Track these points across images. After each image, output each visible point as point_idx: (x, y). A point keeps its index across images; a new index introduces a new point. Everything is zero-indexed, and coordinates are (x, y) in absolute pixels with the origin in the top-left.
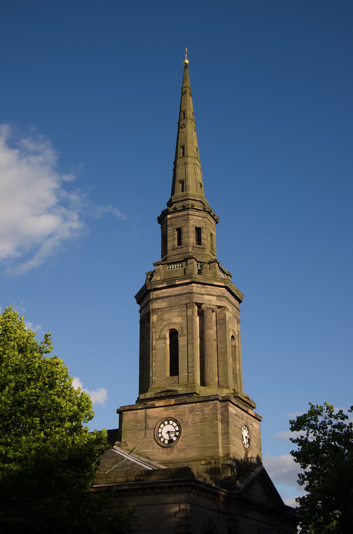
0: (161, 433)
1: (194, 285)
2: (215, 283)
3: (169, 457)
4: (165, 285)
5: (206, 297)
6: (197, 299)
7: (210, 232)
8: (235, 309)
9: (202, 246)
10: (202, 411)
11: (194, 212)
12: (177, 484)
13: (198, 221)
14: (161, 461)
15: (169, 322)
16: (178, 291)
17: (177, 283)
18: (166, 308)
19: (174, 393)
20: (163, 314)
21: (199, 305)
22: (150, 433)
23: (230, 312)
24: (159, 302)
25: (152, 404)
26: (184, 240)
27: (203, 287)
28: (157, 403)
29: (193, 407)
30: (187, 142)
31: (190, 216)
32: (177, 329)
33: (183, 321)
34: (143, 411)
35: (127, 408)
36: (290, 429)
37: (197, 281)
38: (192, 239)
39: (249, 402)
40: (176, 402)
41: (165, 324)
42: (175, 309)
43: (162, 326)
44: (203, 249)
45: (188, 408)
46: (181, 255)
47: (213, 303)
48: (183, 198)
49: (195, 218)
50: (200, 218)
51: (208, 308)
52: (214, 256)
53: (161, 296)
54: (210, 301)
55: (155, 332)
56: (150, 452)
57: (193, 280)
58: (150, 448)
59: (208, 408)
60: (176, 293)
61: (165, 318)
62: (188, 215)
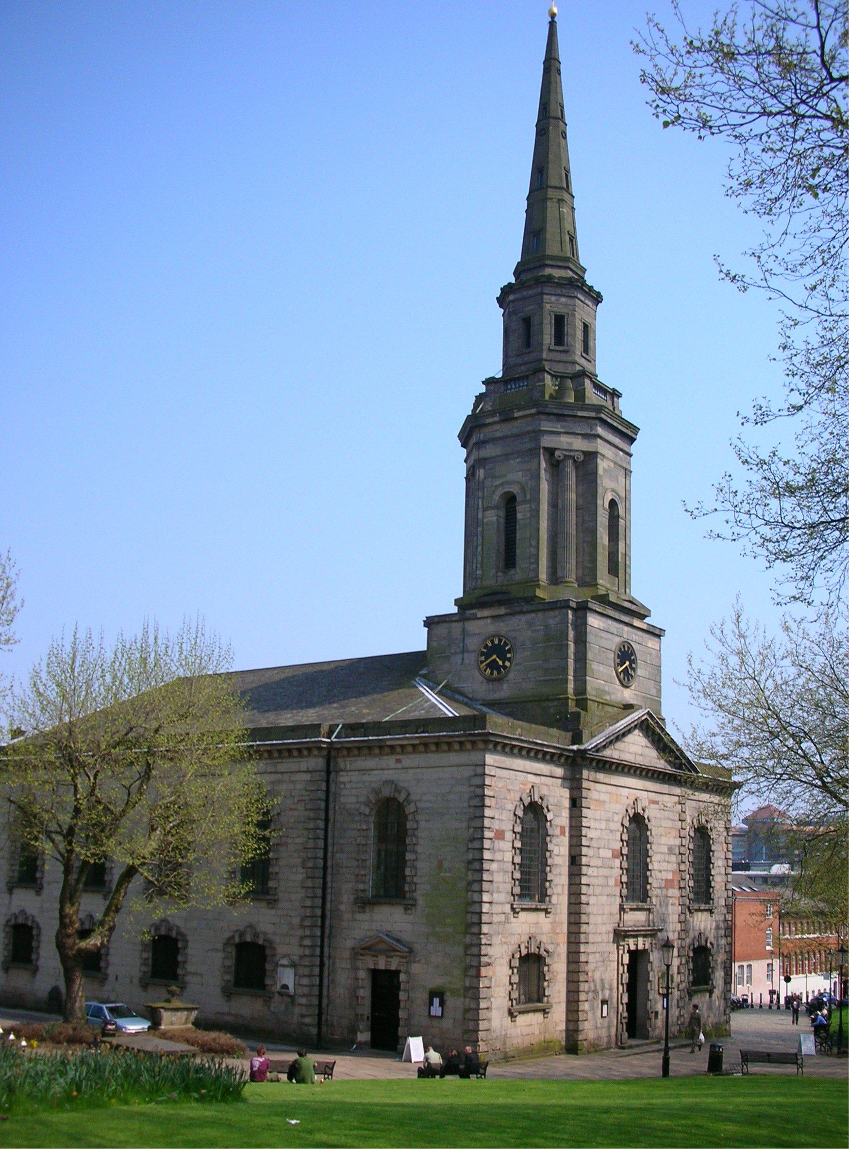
2: (580, 414)
4: (496, 419)
6: (547, 441)
8: (621, 453)
9: (565, 348)
12: (470, 738)
15: (503, 480)
17: (516, 415)
19: (505, 597)
21: (550, 452)
25: (473, 614)
32: (515, 492)
34: (459, 625)
35: (436, 620)
37: (548, 410)
38: (548, 338)
39: (633, 607)
40: (508, 611)
42: (513, 459)
46: (530, 365)
47: (575, 447)
48: (537, 264)
51: (565, 456)
54: (571, 444)
55: (483, 498)
57: (541, 409)
59: (553, 619)
60: (515, 431)
62: (542, 294)
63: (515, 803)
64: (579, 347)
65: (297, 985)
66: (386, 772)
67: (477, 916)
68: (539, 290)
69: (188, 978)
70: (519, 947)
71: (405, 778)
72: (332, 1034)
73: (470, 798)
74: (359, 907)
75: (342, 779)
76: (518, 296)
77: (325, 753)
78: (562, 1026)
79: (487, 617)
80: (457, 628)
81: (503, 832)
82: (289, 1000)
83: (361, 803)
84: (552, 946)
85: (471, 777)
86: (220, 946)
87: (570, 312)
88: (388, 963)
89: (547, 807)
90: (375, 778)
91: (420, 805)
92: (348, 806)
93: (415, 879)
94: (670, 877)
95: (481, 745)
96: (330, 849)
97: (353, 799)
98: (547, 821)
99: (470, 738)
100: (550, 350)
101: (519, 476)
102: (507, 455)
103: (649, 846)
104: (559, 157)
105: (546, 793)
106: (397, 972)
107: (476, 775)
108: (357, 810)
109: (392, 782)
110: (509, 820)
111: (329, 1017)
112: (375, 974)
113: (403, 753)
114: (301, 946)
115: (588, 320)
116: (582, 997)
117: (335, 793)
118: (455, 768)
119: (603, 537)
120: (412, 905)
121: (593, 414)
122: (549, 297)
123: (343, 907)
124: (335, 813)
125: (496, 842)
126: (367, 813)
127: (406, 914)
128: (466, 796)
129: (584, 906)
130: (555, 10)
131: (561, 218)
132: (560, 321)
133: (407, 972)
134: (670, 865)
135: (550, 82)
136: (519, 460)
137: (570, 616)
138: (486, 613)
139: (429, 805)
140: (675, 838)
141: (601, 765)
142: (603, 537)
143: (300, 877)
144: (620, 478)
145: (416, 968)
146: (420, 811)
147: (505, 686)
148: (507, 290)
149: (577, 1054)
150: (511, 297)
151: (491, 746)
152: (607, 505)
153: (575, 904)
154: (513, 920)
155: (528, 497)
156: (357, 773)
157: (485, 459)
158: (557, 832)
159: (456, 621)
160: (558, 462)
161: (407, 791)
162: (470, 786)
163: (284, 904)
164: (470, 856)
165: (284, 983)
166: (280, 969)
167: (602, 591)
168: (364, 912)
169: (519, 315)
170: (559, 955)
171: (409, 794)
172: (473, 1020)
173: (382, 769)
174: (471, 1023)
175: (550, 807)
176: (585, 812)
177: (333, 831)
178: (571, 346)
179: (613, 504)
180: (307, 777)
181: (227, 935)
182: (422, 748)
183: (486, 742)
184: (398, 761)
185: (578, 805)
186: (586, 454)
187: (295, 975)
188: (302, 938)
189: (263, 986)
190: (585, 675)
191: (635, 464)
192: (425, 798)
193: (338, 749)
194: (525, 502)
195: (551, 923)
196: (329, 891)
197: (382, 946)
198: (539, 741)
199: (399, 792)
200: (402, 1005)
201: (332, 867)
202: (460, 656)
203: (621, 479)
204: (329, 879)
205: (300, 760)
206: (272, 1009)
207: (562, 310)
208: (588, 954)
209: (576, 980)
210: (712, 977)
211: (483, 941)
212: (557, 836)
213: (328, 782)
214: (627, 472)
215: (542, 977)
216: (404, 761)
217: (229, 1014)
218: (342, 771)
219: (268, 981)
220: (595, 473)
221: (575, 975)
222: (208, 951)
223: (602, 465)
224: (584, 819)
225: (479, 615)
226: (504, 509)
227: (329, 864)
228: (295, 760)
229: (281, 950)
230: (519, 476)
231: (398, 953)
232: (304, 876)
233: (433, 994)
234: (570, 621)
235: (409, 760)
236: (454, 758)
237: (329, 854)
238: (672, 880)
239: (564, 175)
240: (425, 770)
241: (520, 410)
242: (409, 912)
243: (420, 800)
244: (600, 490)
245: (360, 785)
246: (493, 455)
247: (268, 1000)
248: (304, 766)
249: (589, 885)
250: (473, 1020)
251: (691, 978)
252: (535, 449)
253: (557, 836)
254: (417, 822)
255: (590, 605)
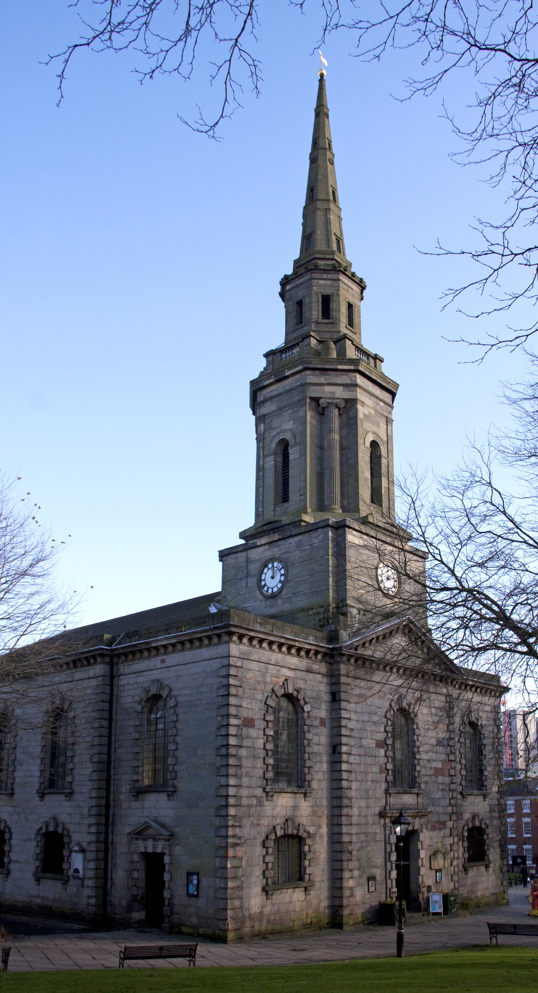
0: (264, 580)
1: (308, 372)
2: (340, 367)
3: (272, 611)
4: (272, 380)
5: (327, 389)
6: (313, 392)
7: (347, 300)
8: (382, 404)
9: (331, 321)
10: (311, 545)
11: (320, 274)
13: (326, 286)
14: (269, 615)
15: (278, 430)
16: (289, 385)
17: (287, 374)
18: (275, 411)
20: (272, 421)
21: (316, 400)
22: (252, 581)
23: (368, 406)
24: (267, 405)
25: (253, 543)
26: (306, 315)
27: (323, 375)
28: (259, 542)
29: (301, 540)
30: (317, 182)
31: (313, 281)
32: (288, 438)
33: (295, 426)
35: (226, 552)
36: (219, 551)
37: (312, 366)
40: (280, 537)
41: (274, 433)
42: (286, 411)
43: (271, 438)
44: (332, 325)
45: (296, 542)
49: (321, 282)
50: (328, 283)
51: (329, 404)
52: (356, 334)
53: (270, 395)
54: (333, 393)
56: (251, 606)
58: (252, 601)
59: (316, 538)
61: (274, 426)
63: (266, 694)
64: (344, 319)
65: (85, 868)
66: (154, 672)
67: (224, 798)
68: (308, 277)
69: (12, 866)
70: (274, 828)
71: (166, 676)
72: (115, 914)
73: (219, 688)
74: (133, 796)
75: (122, 683)
76: (292, 285)
77: (107, 660)
78: (325, 903)
79: (265, 544)
80: (242, 556)
81: (252, 720)
82: (80, 882)
83: (136, 702)
84: (313, 828)
85: (219, 669)
86: (33, 836)
87: (335, 293)
88: (155, 847)
89: (304, 699)
90: (144, 679)
91: (180, 699)
92: (126, 706)
93: (176, 768)
94: (439, 765)
95: (225, 638)
96: (113, 746)
97: (130, 700)
98: (304, 711)
99: (215, 632)
100: (317, 323)
101: (289, 425)
102: (281, 409)
103: (415, 737)
104: (326, 176)
105: (302, 686)
106: (162, 854)
107: (223, 667)
108: (132, 708)
109: (158, 680)
110: (260, 709)
111: (112, 898)
112: (146, 856)
113: (165, 653)
114: (88, 833)
115: (354, 301)
116: (346, 875)
117: (117, 695)
118: (205, 663)
119: (365, 472)
120: (173, 792)
121: (352, 367)
122: (316, 281)
123: (122, 797)
124: (116, 713)
125: (244, 729)
126: (139, 711)
127: (169, 800)
128: (215, 687)
129: (345, 791)
130: (325, 72)
131: (327, 223)
132: (326, 301)
133: (170, 855)
134: (439, 755)
135: (319, 123)
136: (290, 411)
137: (330, 533)
138: (264, 540)
139: (186, 698)
140: (444, 731)
141: (360, 662)
142: (365, 472)
143: (88, 771)
144: (381, 424)
145: (178, 850)
146: (179, 705)
147: (280, 601)
148: (285, 281)
149: (226, 943)
150: (288, 287)
151: (235, 638)
152: (368, 444)
153: (337, 789)
154: (266, 803)
155: (298, 441)
156: (132, 675)
157: (264, 416)
158: (317, 722)
159: (241, 551)
160: (324, 409)
161: (169, 687)
162: (219, 677)
163: (76, 797)
164: (219, 743)
165: (75, 867)
166: (73, 855)
167: (363, 514)
168: (137, 801)
169: (294, 300)
170: (321, 837)
171: (171, 690)
172: (222, 899)
173: (152, 670)
174: (221, 902)
175: (307, 700)
176: (344, 704)
177: (116, 729)
178: (336, 319)
179: (374, 445)
180: (94, 682)
181: (38, 826)
182: (179, 647)
183: (231, 634)
184: (163, 661)
185: (337, 698)
186: (347, 401)
187: (84, 860)
188: (90, 826)
189: (61, 871)
190: (346, 585)
191: (395, 415)
192: (183, 692)
193: (118, 656)
194: (296, 444)
195: (312, 807)
196: (112, 782)
197: (150, 832)
198: (288, 637)
199: (164, 689)
200: (167, 885)
201: (114, 761)
202: (245, 581)
203: (383, 426)
204: (112, 772)
205: (89, 668)
206: (68, 891)
207: (328, 292)
208: (351, 834)
209: (339, 858)
210: (487, 853)
211: (230, 823)
212: (316, 727)
213: (111, 685)
214: (389, 421)
215: (303, 857)
216: (167, 660)
217: (38, 897)
218: (122, 675)
219: (65, 866)
220: (356, 417)
221: (339, 854)
222: (25, 840)
223: (362, 411)
224: (343, 712)
225: (258, 544)
226: (281, 456)
227: (112, 759)
228: (86, 668)
229: (75, 837)
230: (289, 425)
231: (162, 837)
232: (91, 770)
233: (189, 874)
234: (330, 538)
235: (173, 659)
236: (205, 652)
237: (113, 750)
238: (442, 769)
239: (331, 192)
240: (183, 667)
241: (289, 369)
242: (172, 798)
243: (179, 695)
244: (360, 431)
245: (135, 686)
246: (271, 411)
247: (66, 882)
248: (91, 674)
249: (351, 771)
250: (222, 899)
251: (466, 855)
252: (302, 399)
253: (316, 727)
254: (177, 715)
255: (348, 523)
